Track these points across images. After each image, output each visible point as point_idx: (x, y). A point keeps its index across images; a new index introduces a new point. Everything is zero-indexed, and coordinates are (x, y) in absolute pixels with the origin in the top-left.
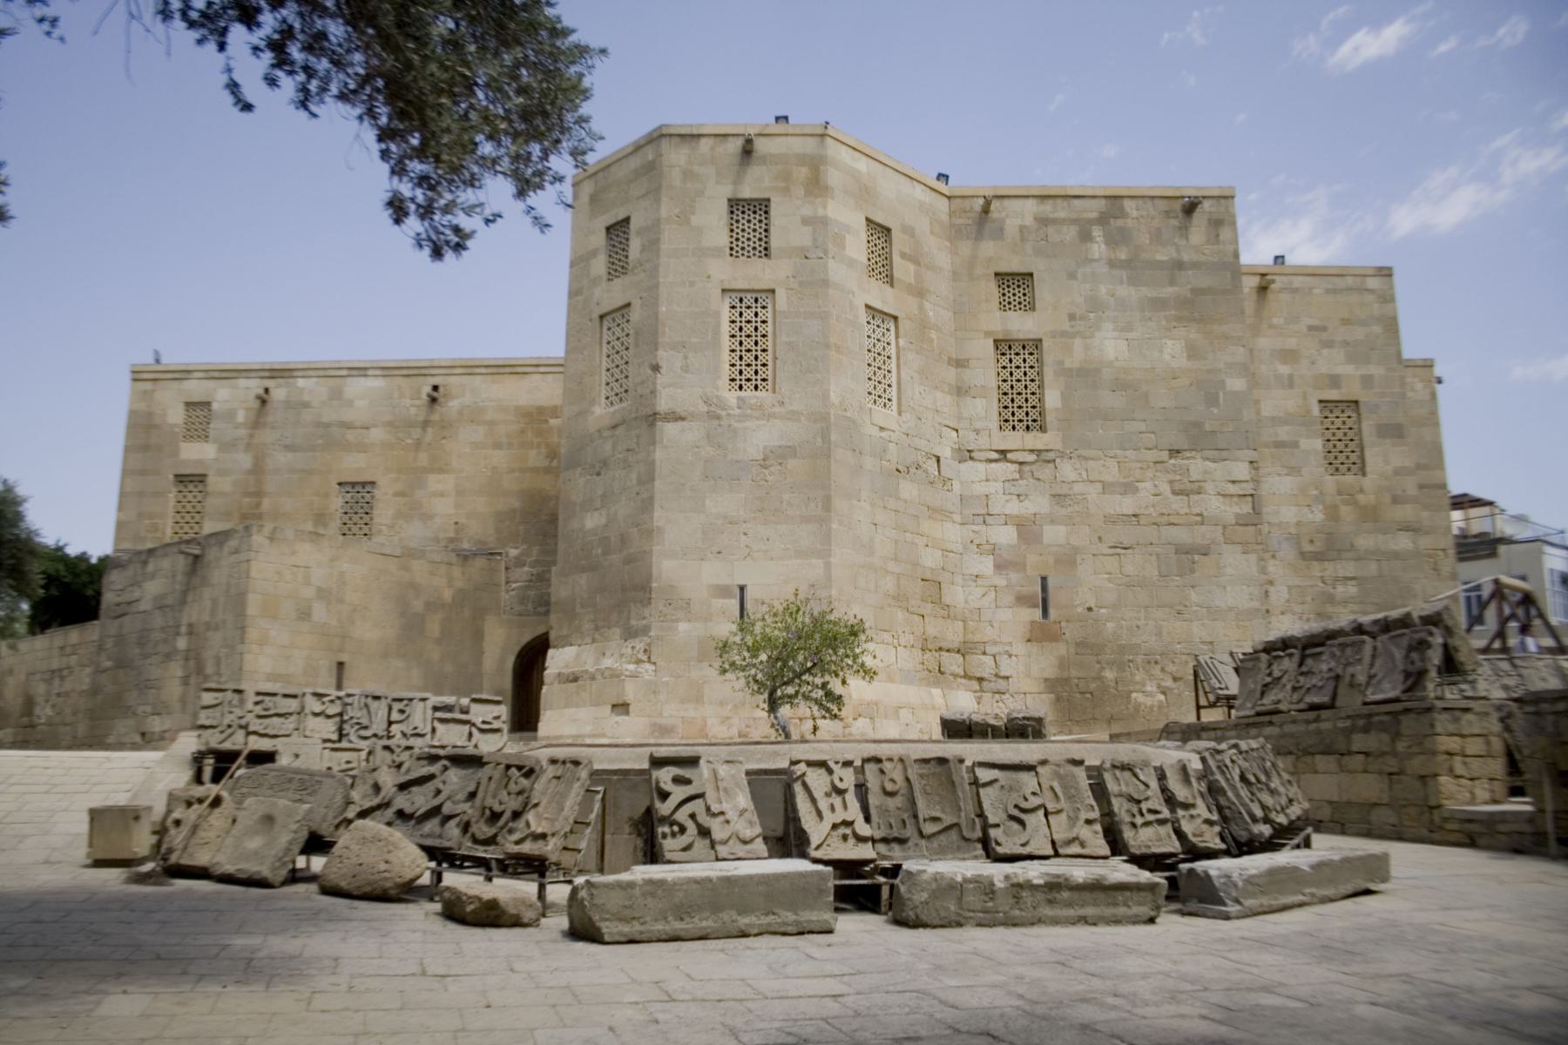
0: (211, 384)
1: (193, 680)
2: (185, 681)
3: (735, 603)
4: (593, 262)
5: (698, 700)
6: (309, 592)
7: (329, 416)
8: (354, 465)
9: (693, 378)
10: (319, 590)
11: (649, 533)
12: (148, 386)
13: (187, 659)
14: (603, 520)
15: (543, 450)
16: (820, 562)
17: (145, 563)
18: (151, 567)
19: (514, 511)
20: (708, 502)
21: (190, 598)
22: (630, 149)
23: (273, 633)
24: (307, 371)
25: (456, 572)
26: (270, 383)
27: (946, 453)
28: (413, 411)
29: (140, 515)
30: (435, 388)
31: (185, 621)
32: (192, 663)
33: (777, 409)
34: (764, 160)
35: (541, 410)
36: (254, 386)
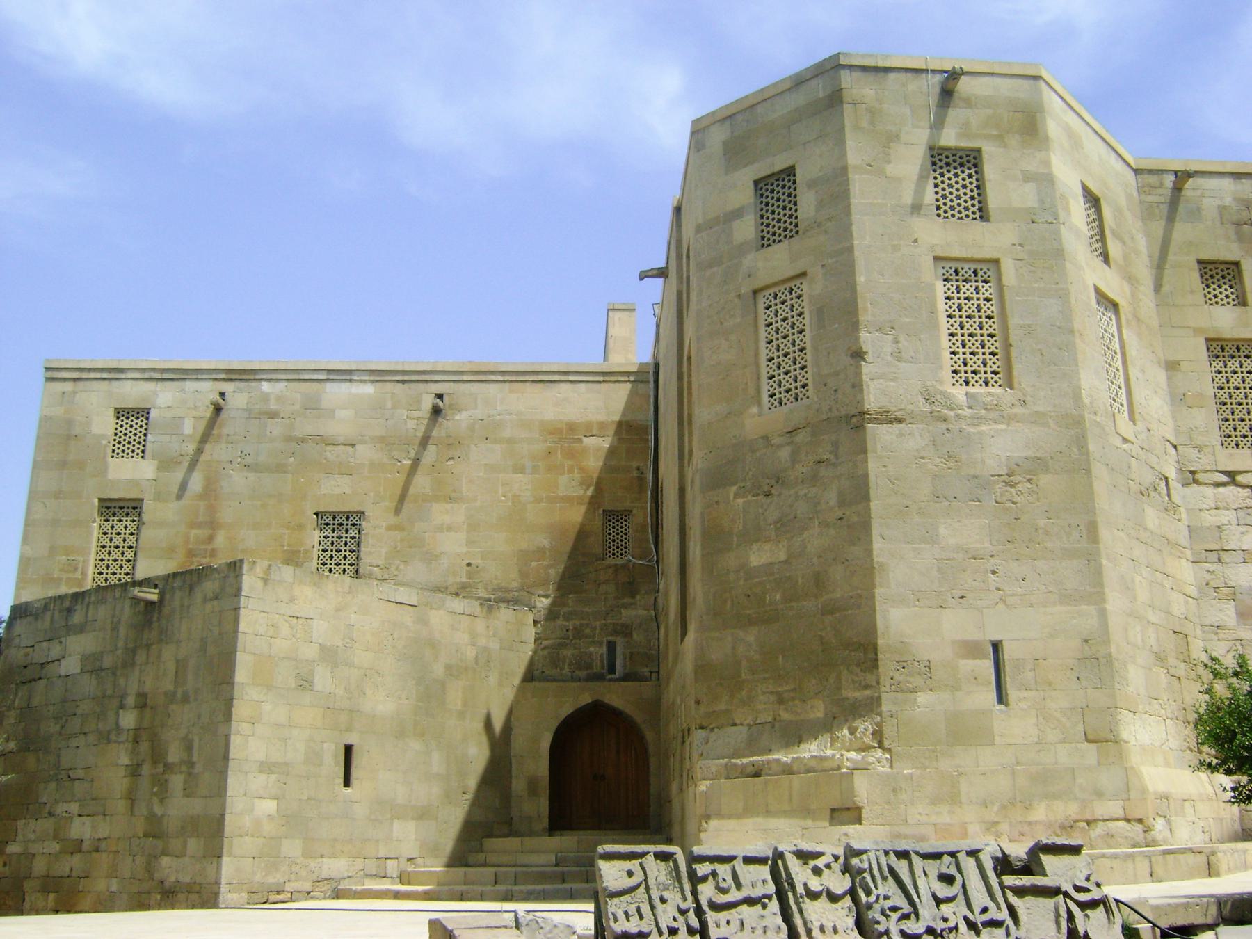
0: (151, 386)
1: (146, 770)
2: (134, 772)
3: (988, 665)
4: (736, 224)
5: (954, 799)
6: (310, 652)
7: (306, 427)
8: (336, 491)
9: (906, 365)
10: (322, 647)
11: (867, 572)
12: (68, 387)
13: (136, 741)
14: (782, 556)
15: (577, 475)
16: (1092, 609)
17: (70, 611)
18: (77, 618)
19: (541, 550)
20: (942, 531)
21: (141, 657)
22: (788, 85)
23: (267, 707)
24: (272, 374)
25: (480, 625)
26: (227, 387)
27: (1172, 474)
28: (411, 424)
29: (53, 550)
30: (440, 396)
31: (133, 688)
32: (144, 747)
33: (1018, 410)
34: (968, 102)
35: (572, 427)
36: (208, 391)
